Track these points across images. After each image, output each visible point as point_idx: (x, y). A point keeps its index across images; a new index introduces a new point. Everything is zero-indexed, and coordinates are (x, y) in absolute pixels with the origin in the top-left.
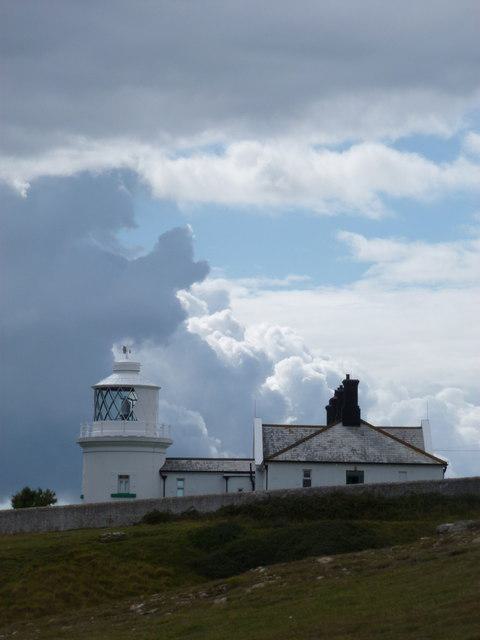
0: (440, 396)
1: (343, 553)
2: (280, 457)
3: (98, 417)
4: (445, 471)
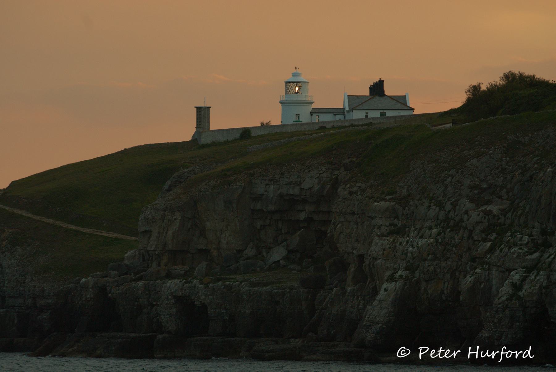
2: (358, 108)
4: (413, 111)
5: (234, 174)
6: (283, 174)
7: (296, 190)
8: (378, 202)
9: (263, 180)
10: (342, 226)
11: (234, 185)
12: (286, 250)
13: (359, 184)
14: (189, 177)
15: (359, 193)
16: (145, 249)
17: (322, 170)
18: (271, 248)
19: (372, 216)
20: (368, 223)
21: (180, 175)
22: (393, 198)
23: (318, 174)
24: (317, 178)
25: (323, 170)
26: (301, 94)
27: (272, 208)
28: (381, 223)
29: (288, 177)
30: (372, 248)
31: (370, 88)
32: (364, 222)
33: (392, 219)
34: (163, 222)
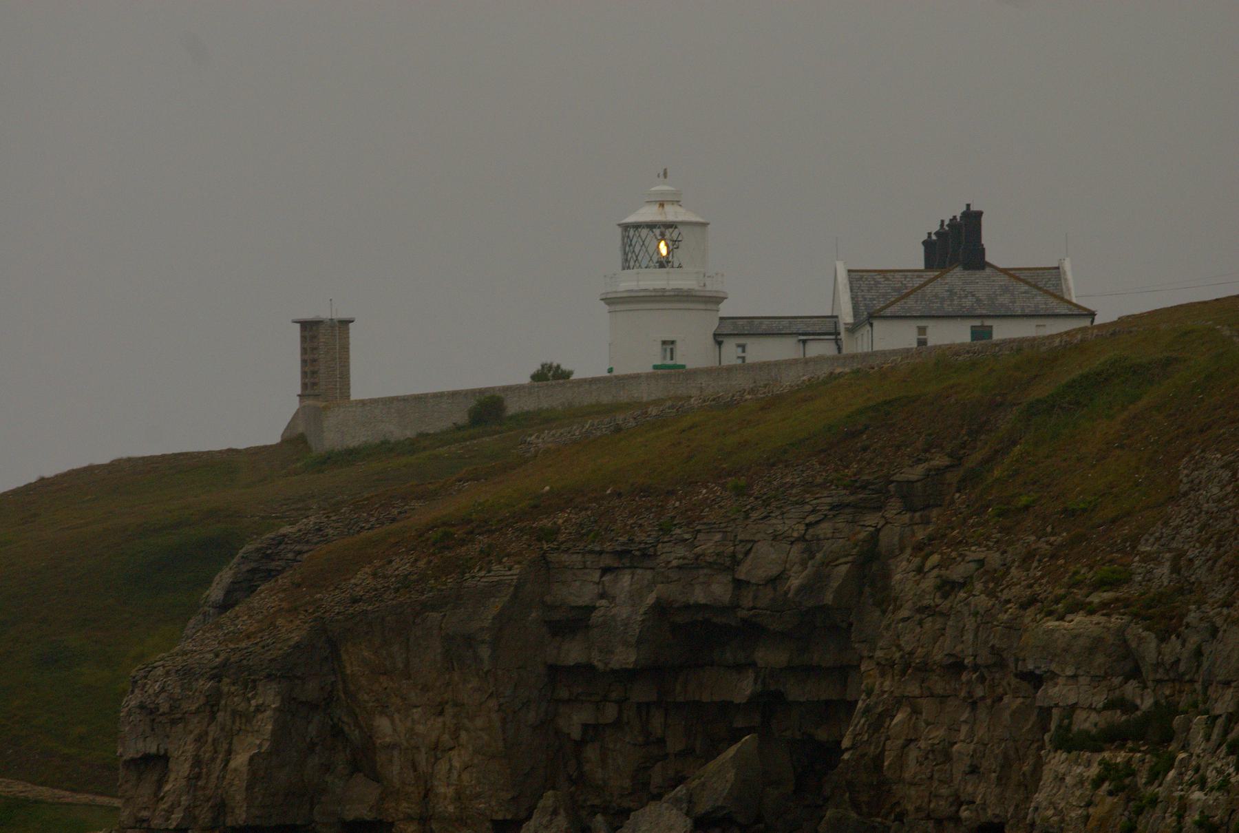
0: (949, 303)
1: (1051, 720)
3: (626, 265)
5: (479, 534)
6: (665, 530)
7: (719, 590)
8: (1061, 618)
9: (591, 552)
10: (914, 718)
11: (482, 573)
12: (687, 814)
13: (975, 553)
14: (300, 553)
15: (979, 586)
16: (145, 825)
17: (813, 511)
18: (625, 813)
19: (1037, 672)
20: (1020, 700)
21: (267, 548)
22: (1117, 600)
23: (802, 527)
24: (798, 539)
25: (820, 510)
26: (680, 267)
27: (625, 657)
28: (1072, 699)
29: (687, 540)
30: (1040, 797)
31: (924, 243)
32: (1001, 699)
33: (1117, 681)
34: (213, 717)
